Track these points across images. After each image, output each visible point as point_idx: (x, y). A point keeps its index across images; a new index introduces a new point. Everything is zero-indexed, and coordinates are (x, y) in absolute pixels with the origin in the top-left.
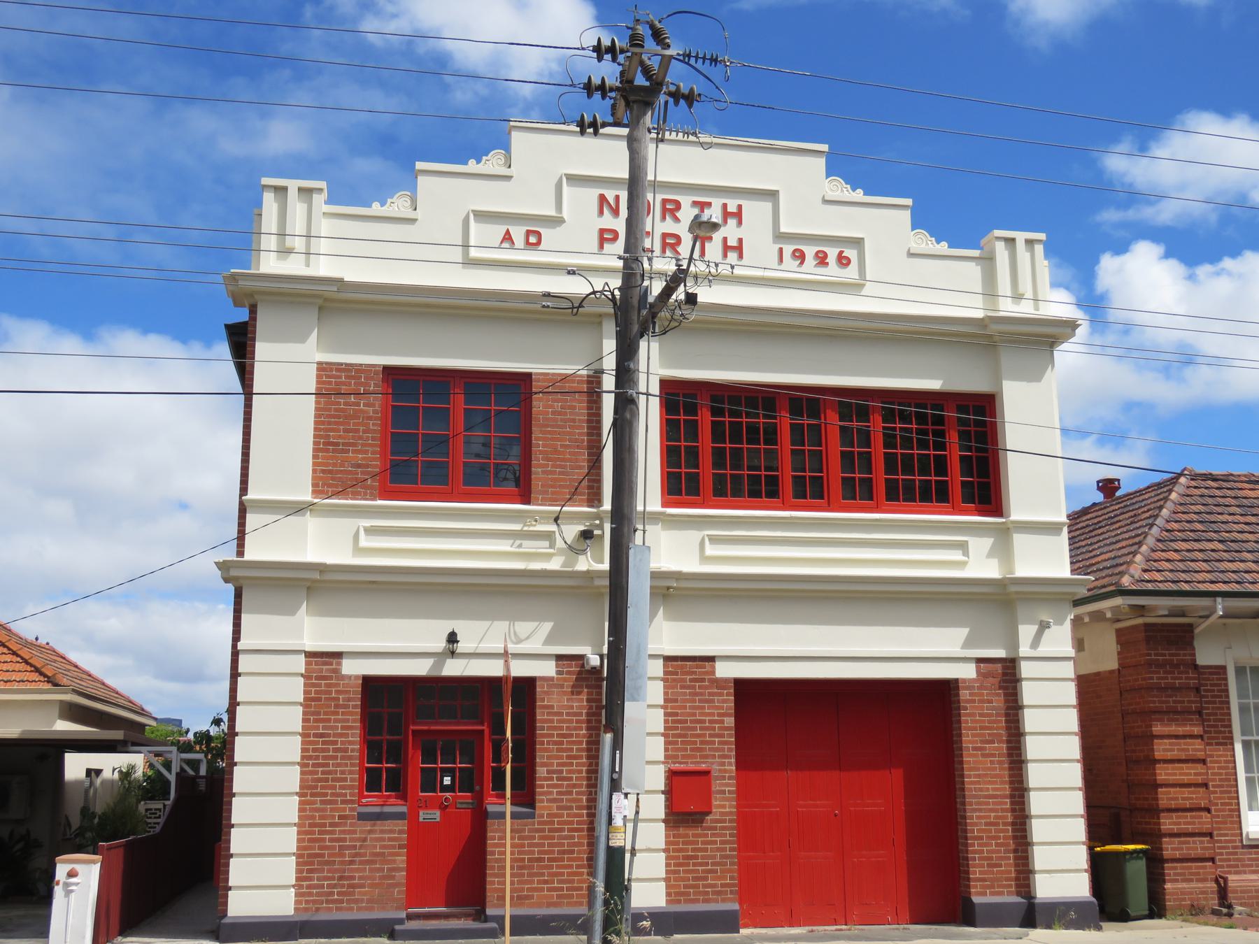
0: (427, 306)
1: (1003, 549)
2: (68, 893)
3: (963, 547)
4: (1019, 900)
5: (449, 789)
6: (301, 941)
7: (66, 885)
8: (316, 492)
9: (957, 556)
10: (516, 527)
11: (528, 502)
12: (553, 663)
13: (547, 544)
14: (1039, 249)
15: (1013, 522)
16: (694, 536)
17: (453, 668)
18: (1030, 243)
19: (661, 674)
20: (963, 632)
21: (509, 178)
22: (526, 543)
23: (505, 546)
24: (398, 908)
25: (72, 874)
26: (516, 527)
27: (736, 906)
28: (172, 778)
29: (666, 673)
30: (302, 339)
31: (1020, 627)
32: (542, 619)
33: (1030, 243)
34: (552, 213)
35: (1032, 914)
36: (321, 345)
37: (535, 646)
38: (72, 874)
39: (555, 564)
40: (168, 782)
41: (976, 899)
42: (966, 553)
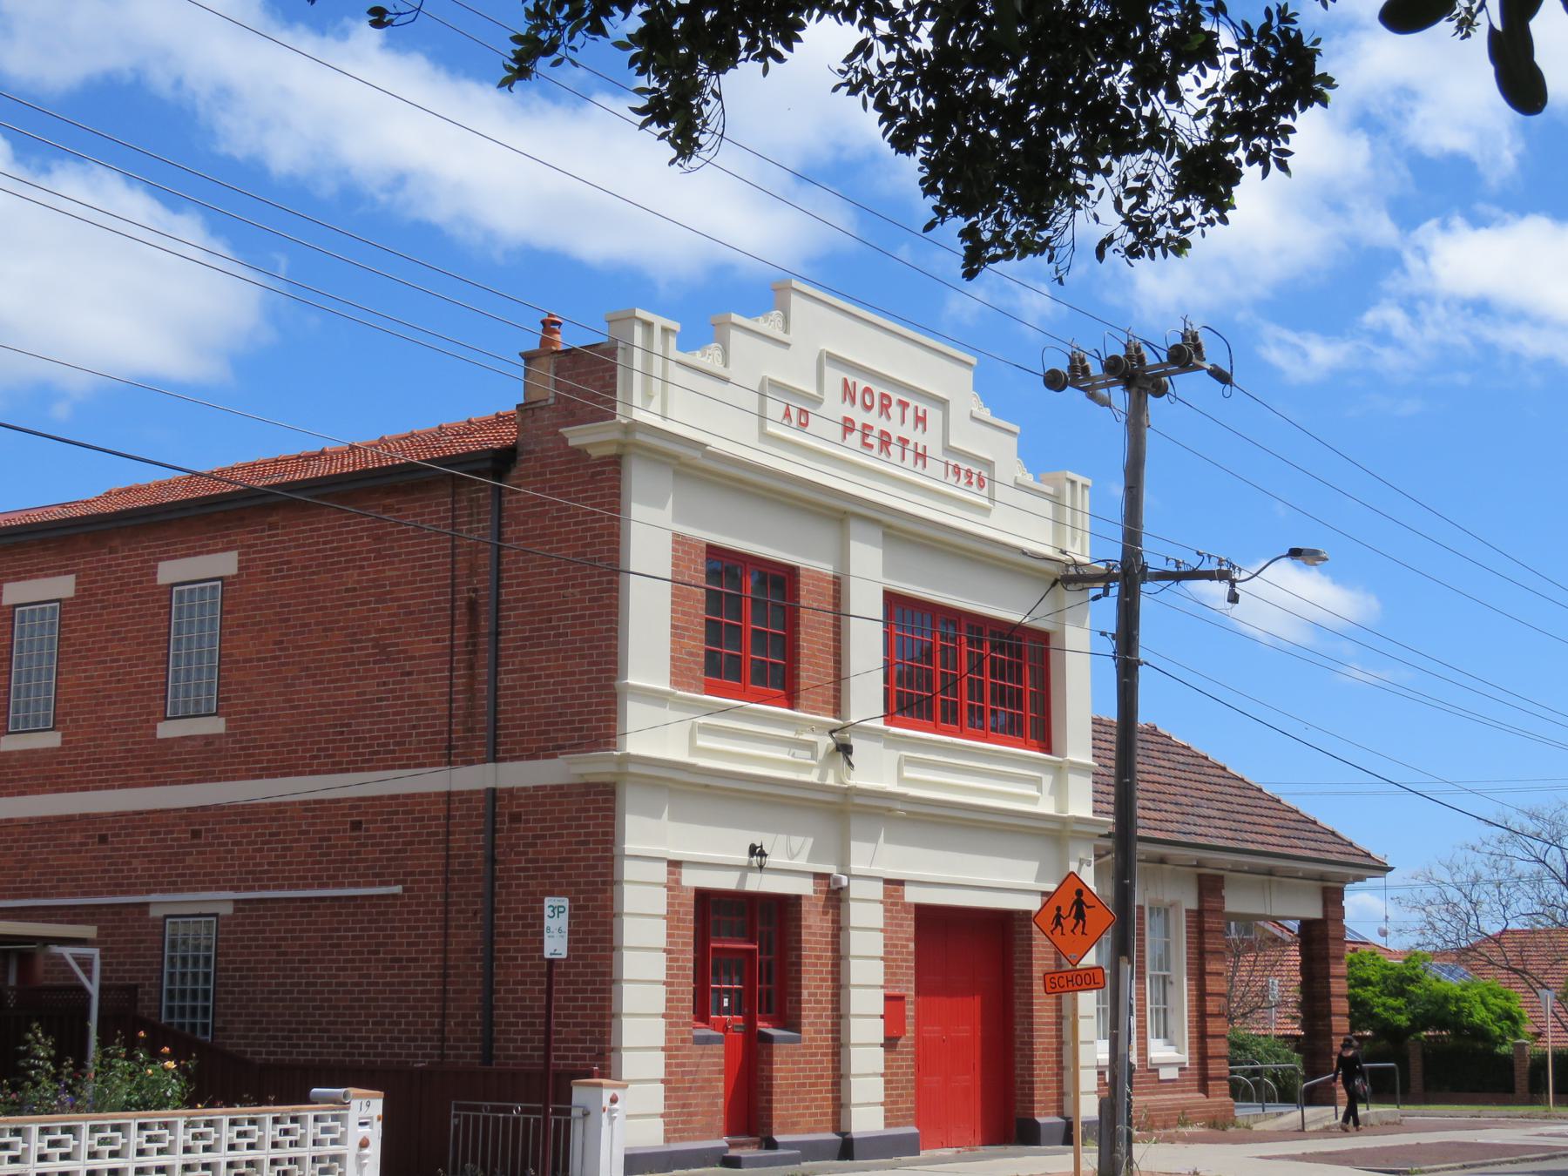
0: (740, 481)
1: (1059, 790)
2: (612, 1119)
3: (1037, 782)
4: (1059, 1120)
5: (729, 1011)
6: (676, 1172)
7: (611, 1111)
8: (674, 683)
9: (1031, 791)
10: (790, 734)
11: (791, 707)
12: (810, 881)
13: (808, 754)
14: (673, 341)
15: (1072, 763)
16: (893, 755)
17: (758, 883)
18: (665, 330)
19: (881, 897)
20: (1033, 866)
21: (787, 345)
22: (799, 753)
23: (782, 754)
24: (719, 1137)
25: (614, 1100)
26: (790, 734)
27: (913, 1130)
28: (94, 989)
29: (886, 896)
30: (662, 506)
31: (854, 844)
32: (805, 834)
33: (665, 330)
34: (814, 391)
35: (847, 1149)
36: (678, 516)
37: (801, 863)
38: (614, 1100)
39: (812, 777)
40: (88, 997)
41: (1040, 1120)
42: (1040, 790)
